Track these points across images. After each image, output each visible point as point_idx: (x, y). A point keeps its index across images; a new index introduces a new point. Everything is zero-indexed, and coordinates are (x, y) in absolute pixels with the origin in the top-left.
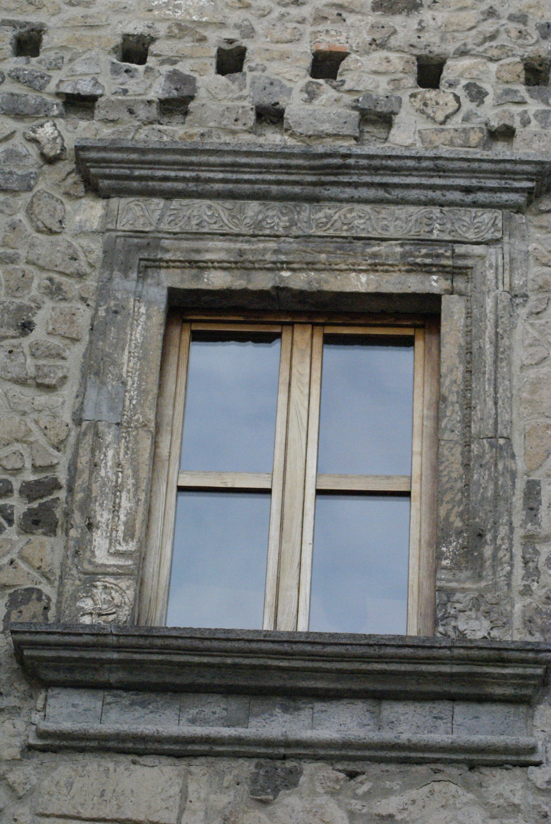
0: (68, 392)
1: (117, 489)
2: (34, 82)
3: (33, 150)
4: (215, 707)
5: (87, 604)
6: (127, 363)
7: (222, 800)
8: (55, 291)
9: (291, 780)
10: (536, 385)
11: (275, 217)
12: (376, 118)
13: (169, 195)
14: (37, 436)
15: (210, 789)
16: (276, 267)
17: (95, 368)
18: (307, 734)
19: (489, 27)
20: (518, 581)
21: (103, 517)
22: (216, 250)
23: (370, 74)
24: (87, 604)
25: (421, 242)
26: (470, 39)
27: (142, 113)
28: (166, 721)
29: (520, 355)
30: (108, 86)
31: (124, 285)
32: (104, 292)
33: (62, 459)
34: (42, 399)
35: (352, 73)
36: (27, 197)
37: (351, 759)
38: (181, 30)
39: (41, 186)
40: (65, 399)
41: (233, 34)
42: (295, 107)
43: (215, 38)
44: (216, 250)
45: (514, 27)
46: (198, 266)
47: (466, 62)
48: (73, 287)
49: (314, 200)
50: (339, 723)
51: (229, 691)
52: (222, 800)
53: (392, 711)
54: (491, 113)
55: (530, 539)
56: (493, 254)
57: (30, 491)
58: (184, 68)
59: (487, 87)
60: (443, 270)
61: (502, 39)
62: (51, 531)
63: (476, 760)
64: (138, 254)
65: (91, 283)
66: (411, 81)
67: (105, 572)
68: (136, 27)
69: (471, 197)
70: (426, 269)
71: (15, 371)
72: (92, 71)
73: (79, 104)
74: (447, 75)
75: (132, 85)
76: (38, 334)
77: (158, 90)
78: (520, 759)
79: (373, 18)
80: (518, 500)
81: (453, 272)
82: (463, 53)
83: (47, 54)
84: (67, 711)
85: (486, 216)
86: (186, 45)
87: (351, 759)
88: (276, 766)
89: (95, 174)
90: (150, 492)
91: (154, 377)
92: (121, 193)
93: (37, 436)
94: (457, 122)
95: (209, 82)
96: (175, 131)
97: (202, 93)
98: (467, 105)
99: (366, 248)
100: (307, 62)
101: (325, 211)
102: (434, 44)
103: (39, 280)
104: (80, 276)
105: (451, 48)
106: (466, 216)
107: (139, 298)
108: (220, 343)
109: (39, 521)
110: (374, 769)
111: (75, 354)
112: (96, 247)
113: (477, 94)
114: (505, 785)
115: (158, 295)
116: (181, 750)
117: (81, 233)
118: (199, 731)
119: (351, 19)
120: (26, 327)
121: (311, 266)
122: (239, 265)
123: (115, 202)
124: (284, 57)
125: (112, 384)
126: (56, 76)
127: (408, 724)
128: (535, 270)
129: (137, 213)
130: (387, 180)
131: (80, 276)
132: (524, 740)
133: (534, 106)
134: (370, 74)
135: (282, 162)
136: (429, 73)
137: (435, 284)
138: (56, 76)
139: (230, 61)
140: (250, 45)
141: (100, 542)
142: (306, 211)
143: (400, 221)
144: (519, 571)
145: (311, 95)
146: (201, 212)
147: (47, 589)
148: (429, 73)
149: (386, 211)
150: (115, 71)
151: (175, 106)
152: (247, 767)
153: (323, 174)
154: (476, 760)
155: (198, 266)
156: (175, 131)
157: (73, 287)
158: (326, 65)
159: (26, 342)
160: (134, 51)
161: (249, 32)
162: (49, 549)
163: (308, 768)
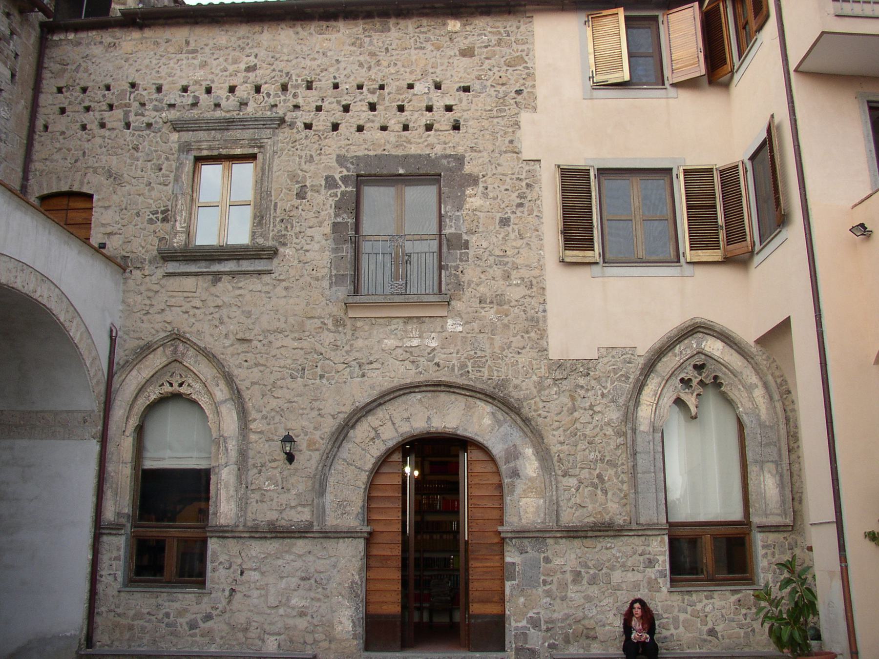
0: (171, 185)
1: (182, 211)
2: (160, 101)
3: (161, 120)
4: (203, 264)
5: (175, 240)
6: (184, 177)
7: (205, 285)
8: (167, 159)
9: (220, 280)
10: (278, 176)
11: (218, 135)
12: (243, 104)
13: (193, 131)
14: (164, 198)
15: (203, 283)
16: (219, 149)
17: (177, 179)
18: (222, 270)
19: (273, 74)
20: (271, 228)
21: (178, 218)
22: (204, 145)
23: (243, 91)
24: (175, 240)
25: (252, 140)
26: (267, 78)
27: (186, 108)
28: (193, 268)
29: (275, 169)
30: (178, 101)
31: (183, 156)
32: (178, 159)
33: (169, 203)
34: (165, 188)
35: (238, 92)
36: (159, 134)
37: (233, 274)
38: (196, 82)
39: (163, 130)
40: (169, 188)
41: (208, 82)
42: (223, 103)
43: (204, 84)
44: (204, 145)
45: (280, 73)
46: (201, 150)
47: (267, 85)
48: (171, 157)
49: (227, 129)
50: (230, 266)
51: (206, 260)
52: (205, 285)
53: (242, 262)
54: (272, 101)
55: (274, 217)
56: (270, 142)
57: (163, 212)
58: (196, 94)
59: (271, 93)
60: (258, 147)
61: (276, 78)
62: (168, 222)
63: (260, 273)
64: (185, 148)
65: (176, 156)
66: (253, 92)
67: (178, 232)
68: (185, 83)
69: (265, 126)
70: (254, 147)
71: (158, 181)
72: (173, 96)
73: (171, 106)
74: (262, 90)
75: (184, 100)
76: (163, 171)
77: (190, 102)
78: (269, 272)
79: (244, 74)
80: (272, 207)
81: (260, 147)
82: (266, 83)
83: (164, 92)
84: (172, 267)
85: (268, 131)
86: (197, 87)
87: (233, 274)
88: (217, 277)
89: (177, 127)
90: (191, 209)
91: (191, 180)
92: (182, 131)
93: (164, 198)
94: (263, 104)
95: (203, 97)
96: (195, 113)
97: (201, 101)
98: (266, 98)
99: (240, 140)
100: (227, 89)
101: (230, 133)
102: (259, 81)
103: (163, 156)
104: (173, 154)
105: (263, 81)
106: (264, 131)
107: (187, 159)
108: (111, 413)
109: (165, 220)
110: (238, 276)
111: (172, 175)
112: (176, 146)
113: (268, 95)
114: (266, 278)
115: (191, 158)
116: (196, 274)
117: (173, 142)
118: (199, 270)
119: (239, 74)
120: (161, 169)
121: (227, 148)
122: (210, 148)
123: (182, 133)
124: (221, 88)
125: (180, 184)
126: (166, 99)
127: (246, 265)
128: (280, 145)
129: (187, 136)
130: (243, 123)
131: (173, 154)
132: (270, 268)
133: (283, 98)
134: (243, 91)
135: (219, 121)
136: (258, 90)
137: (256, 150)
138: (166, 99)
139: (209, 91)
140: (213, 86)
141: (178, 224)
142: (226, 133)
143: (247, 134)
144: (272, 225)
145: (228, 98)
146: (202, 135)
147: (167, 237)
148: (258, 90)
149: (245, 131)
150: (180, 96)
151: (195, 105)
152: (211, 277)
153: (228, 124)
154: (260, 273)
155: (201, 150)
156: (195, 113)
157: (171, 157)
158: (232, 89)
159: (160, 173)
160: (185, 89)
161: (213, 81)
162: (167, 226)
163: (224, 276)
